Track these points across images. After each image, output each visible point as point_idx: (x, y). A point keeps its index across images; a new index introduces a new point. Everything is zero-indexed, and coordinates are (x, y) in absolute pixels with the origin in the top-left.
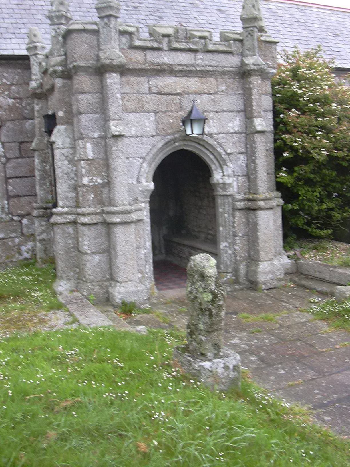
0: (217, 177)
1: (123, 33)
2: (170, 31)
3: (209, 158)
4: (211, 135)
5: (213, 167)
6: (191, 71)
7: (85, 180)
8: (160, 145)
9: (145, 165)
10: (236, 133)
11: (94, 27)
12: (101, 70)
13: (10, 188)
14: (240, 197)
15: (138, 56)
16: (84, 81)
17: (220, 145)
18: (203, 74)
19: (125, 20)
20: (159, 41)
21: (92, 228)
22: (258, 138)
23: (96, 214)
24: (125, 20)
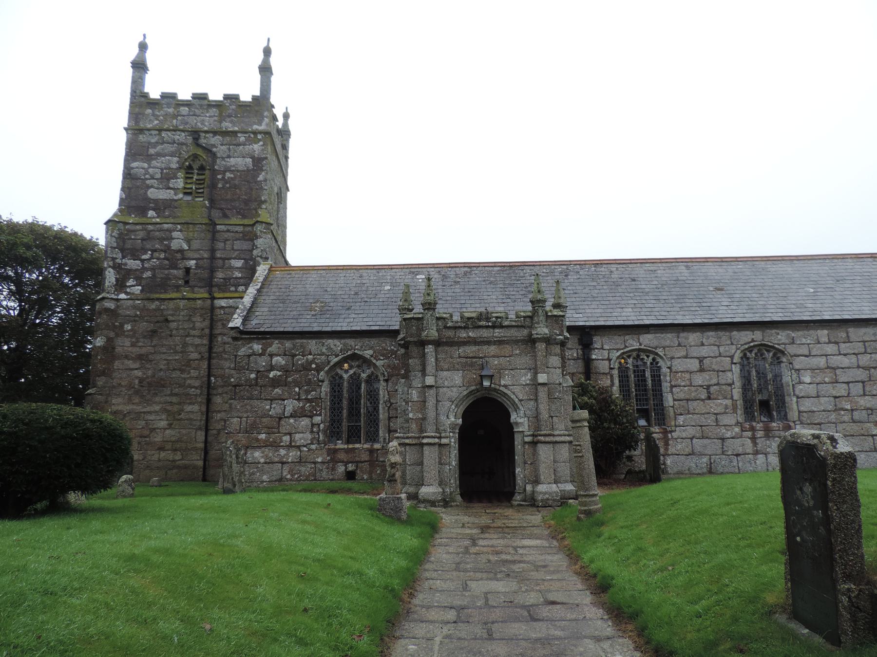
0: (514, 417)
1: (438, 319)
2: (474, 315)
3: (507, 404)
4: (505, 386)
5: (510, 410)
6: (483, 342)
7: (411, 415)
8: (465, 393)
9: (453, 407)
10: (527, 385)
11: (420, 316)
12: (423, 344)
13: (392, 424)
14: (529, 433)
15: (450, 333)
16: (414, 350)
17: (514, 393)
18: (500, 342)
19: (441, 310)
20: (470, 323)
21: (412, 448)
22: (540, 388)
23: (415, 438)
24: (441, 310)
